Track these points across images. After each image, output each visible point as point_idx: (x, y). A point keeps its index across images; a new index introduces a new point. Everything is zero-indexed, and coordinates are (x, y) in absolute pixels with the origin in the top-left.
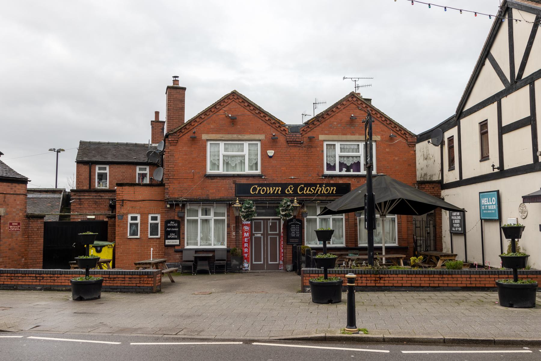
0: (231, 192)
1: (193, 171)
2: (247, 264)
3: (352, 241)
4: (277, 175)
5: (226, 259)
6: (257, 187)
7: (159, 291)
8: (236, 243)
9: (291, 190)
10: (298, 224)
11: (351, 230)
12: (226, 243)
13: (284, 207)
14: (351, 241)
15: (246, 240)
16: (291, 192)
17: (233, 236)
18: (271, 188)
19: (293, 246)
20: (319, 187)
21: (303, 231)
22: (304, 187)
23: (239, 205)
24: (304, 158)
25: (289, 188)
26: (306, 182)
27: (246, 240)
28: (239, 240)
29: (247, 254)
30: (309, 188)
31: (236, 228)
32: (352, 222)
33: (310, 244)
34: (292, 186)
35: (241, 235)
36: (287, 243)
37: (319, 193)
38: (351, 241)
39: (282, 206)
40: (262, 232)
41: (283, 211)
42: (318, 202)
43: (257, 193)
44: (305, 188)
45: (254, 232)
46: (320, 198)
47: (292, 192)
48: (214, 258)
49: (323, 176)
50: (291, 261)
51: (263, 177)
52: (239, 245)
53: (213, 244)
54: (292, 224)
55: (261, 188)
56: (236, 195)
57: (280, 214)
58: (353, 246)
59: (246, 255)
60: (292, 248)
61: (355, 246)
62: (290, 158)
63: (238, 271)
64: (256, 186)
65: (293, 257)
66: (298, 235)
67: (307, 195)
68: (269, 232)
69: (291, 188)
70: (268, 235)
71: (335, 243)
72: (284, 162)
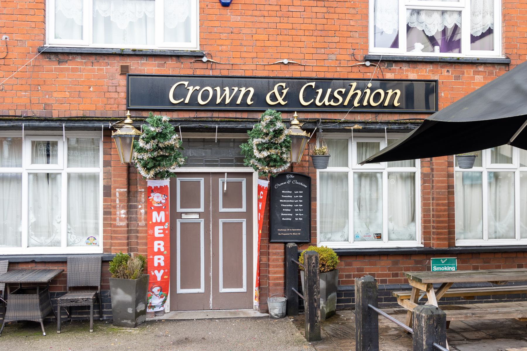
0: (115, 99)
1: (4, 37)
2: (162, 297)
3: (441, 234)
4: (244, 55)
5: (98, 284)
6: (189, 85)
7: (19, 322)
8: (128, 238)
9: (281, 94)
10: (299, 188)
11: (438, 205)
12: (100, 239)
13: (267, 134)
14: (438, 234)
15: (157, 231)
16: (280, 100)
17: (121, 220)
18: (227, 89)
19: (285, 248)
20: (355, 90)
21: (312, 207)
22: (317, 87)
23: (133, 132)
24: (315, 9)
25: (276, 90)
26: (322, 75)
27: (157, 231)
28: (137, 232)
29: (162, 271)
30: (329, 90)
31: (128, 196)
32: (442, 182)
33: (329, 240)
34: (284, 85)
35: (143, 216)
36: (270, 238)
37: (356, 104)
38: (438, 234)
39: (259, 133)
40: (202, 209)
41: (262, 147)
42: (356, 126)
43: (187, 101)
44: (320, 91)
45: (179, 210)
46: (359, 118)
47: (284, 100)
48: (65, 282)
49: (366, 60)
50: (282, 287)
51: (205, 59)
52: (137, 244)
53: (64, 243)
54: (284, 188)
55: (198, 88)
56: (128, 105)
57: (251, 156)
58: (444, 246)
59: (159, 275)
60: (283, 251)
61: (449, 246)
62: (278, 8)
63: (129, 322)
64: (186, 83)
65: (285, 277)
66: (298, 217)
67: (325, 109)
68: (222, 210)
69: (281, 89)
70: (218, 215)
71: (393, 236)
72: (262, 19)
